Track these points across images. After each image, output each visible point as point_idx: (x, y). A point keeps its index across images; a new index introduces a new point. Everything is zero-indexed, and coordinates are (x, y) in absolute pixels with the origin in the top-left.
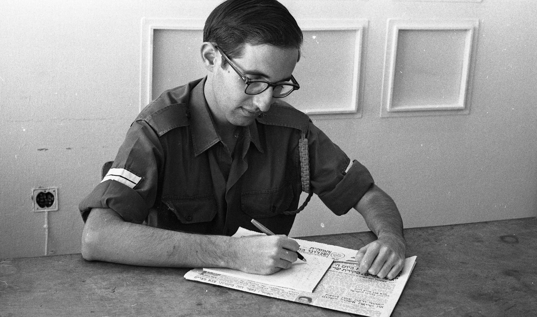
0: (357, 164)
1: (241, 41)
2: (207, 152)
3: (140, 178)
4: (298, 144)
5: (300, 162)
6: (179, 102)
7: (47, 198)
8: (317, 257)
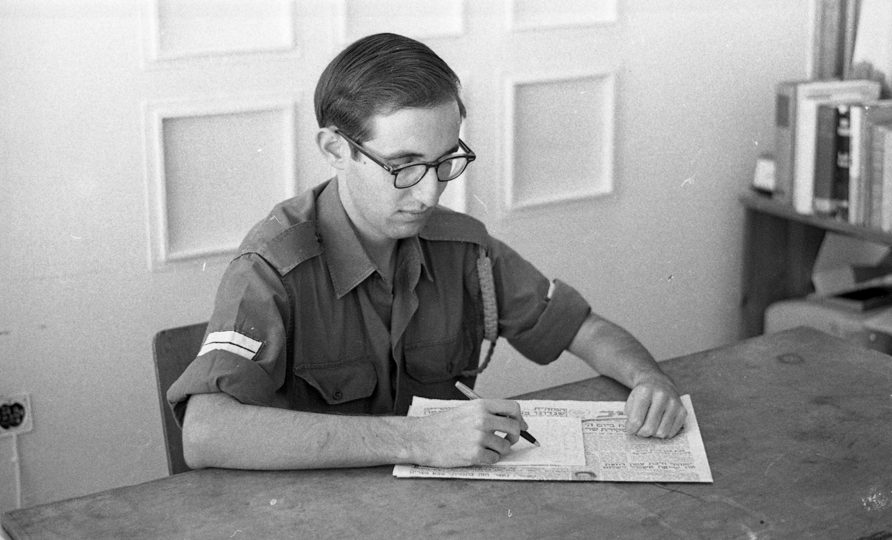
0: (561, 286)
1: (369, 113)
2: (355, 291)
3: (260, 343)
4: (476, 267)
5: (480, 293)
6: (304, 220)
7: (12, 412)
8: (555, 418)
